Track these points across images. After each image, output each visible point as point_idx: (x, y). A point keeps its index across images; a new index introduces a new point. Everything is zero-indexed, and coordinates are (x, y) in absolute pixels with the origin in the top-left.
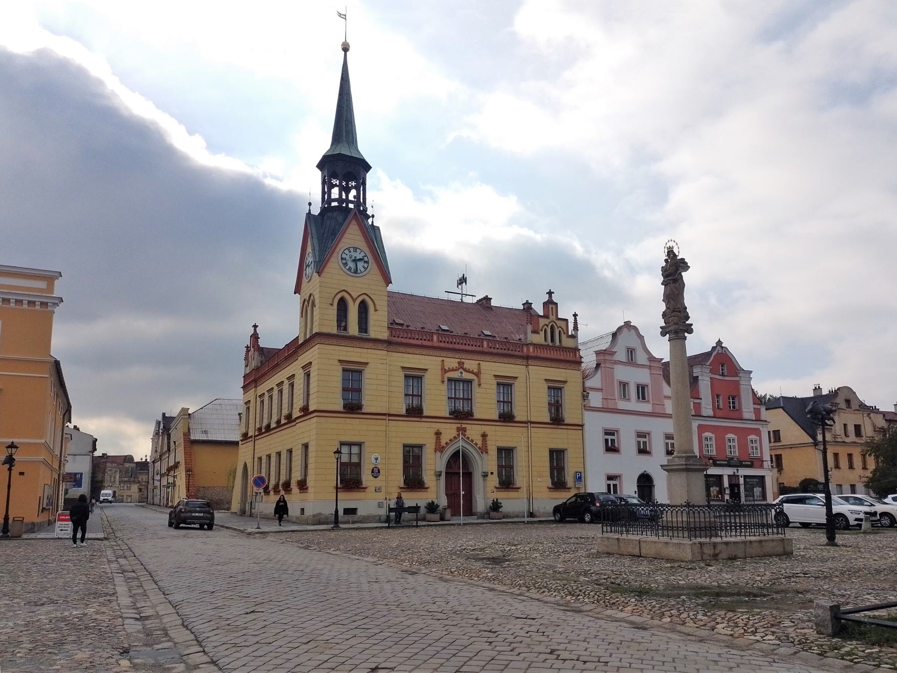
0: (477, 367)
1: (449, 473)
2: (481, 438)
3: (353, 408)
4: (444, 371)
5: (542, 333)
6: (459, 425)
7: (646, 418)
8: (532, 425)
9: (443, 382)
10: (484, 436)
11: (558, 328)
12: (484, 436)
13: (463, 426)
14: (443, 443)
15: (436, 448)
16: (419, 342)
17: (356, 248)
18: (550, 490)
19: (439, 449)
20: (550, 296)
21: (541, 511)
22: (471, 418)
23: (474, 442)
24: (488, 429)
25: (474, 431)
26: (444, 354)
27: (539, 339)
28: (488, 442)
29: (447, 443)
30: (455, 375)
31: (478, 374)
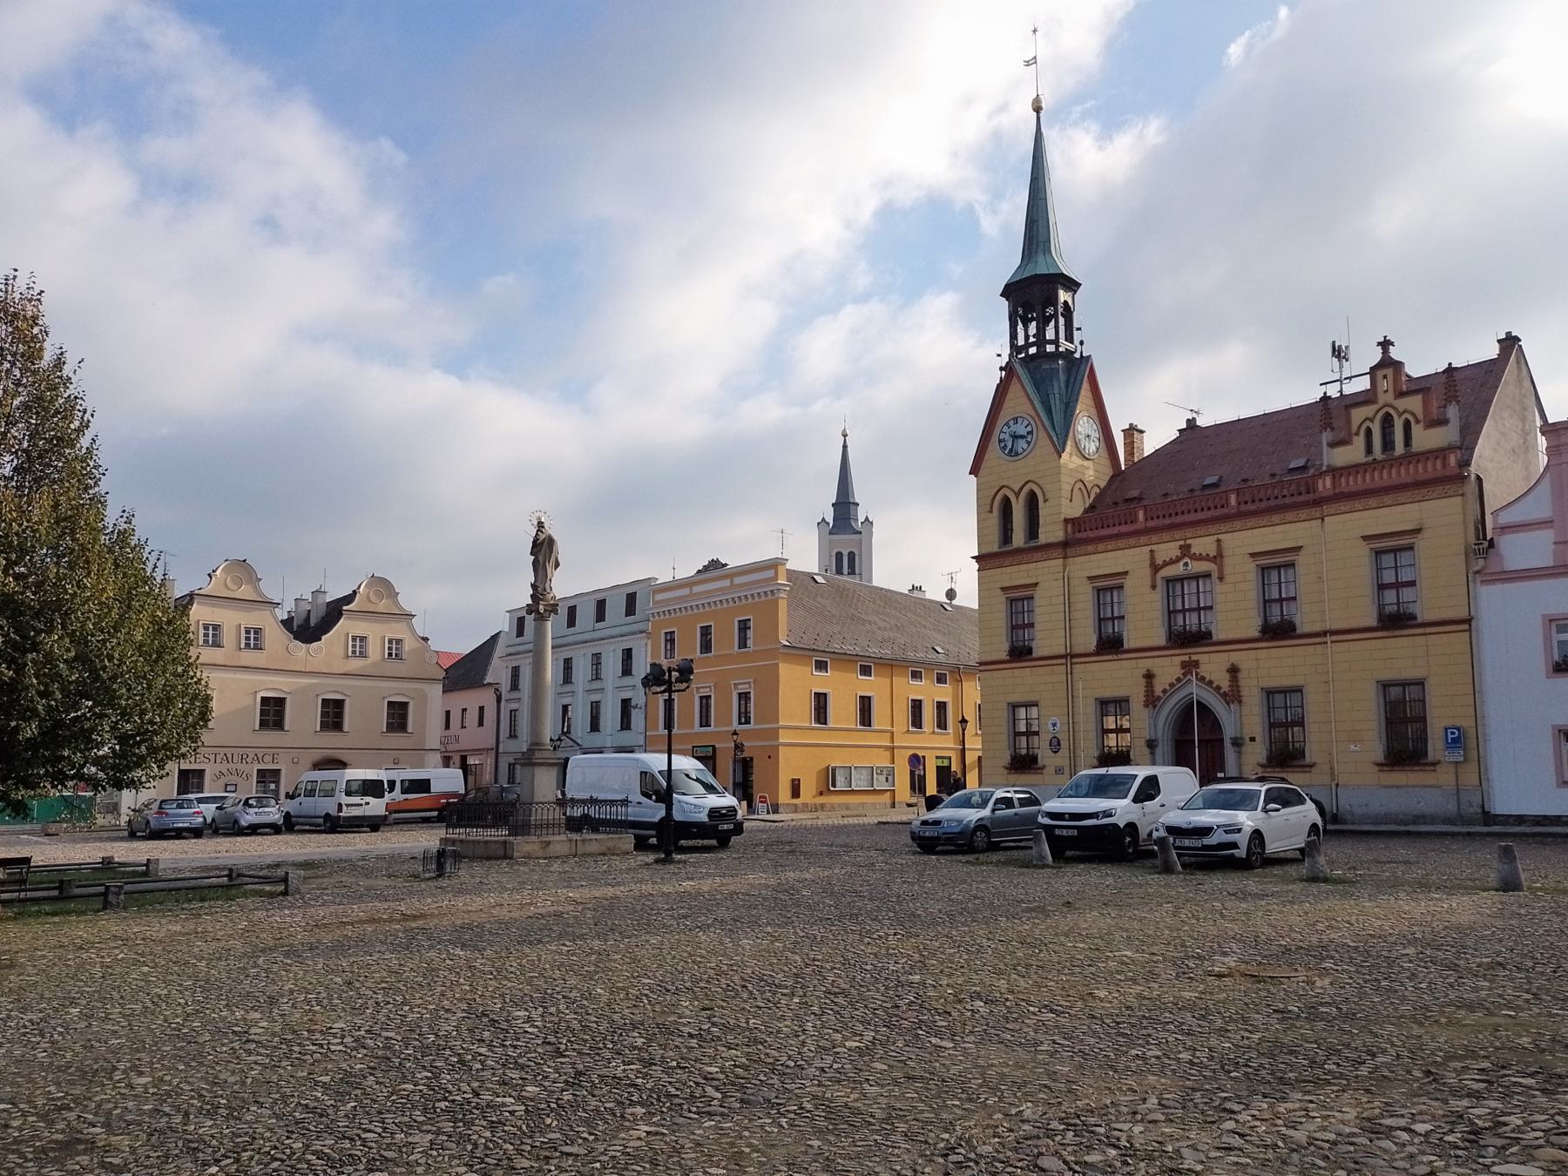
0: (1214, 546)
1: (1208, 741)
2: (1227, 676)
3: (1395, 621)
4: (1155, 568)
5: (1360, 441)
6: (1186, 658)
7: (1532, 582)
8: (1075, 660)
9: (1154, 587)
10: (1234, 671)
11: (1400, 415)
12: (1234, 671)
13: (1194, 658)
14: (1158, 690)
15: (1147, 700)
16: (1115, 530)
17: (1017, 418)
18: (1381, 768)
19: (1151, 701)
20: (1385, 351)
21: (1359, 811)
22: (1029, 657)
23: (1168, 688)
24: (1242, 658)
25: (1213, 665)
26: (1212, 529)
27: (1352, 453)
28: (1242, 683)
29: (1165, 691)
30: (1178, 570)
31: (1218, 558)
